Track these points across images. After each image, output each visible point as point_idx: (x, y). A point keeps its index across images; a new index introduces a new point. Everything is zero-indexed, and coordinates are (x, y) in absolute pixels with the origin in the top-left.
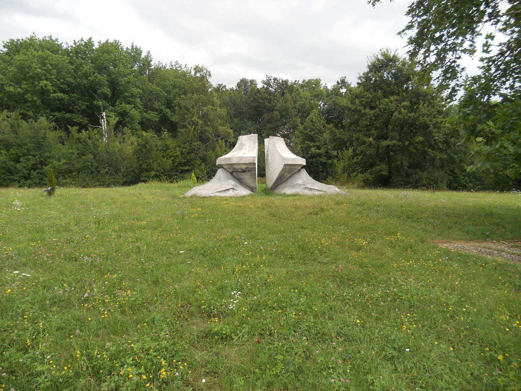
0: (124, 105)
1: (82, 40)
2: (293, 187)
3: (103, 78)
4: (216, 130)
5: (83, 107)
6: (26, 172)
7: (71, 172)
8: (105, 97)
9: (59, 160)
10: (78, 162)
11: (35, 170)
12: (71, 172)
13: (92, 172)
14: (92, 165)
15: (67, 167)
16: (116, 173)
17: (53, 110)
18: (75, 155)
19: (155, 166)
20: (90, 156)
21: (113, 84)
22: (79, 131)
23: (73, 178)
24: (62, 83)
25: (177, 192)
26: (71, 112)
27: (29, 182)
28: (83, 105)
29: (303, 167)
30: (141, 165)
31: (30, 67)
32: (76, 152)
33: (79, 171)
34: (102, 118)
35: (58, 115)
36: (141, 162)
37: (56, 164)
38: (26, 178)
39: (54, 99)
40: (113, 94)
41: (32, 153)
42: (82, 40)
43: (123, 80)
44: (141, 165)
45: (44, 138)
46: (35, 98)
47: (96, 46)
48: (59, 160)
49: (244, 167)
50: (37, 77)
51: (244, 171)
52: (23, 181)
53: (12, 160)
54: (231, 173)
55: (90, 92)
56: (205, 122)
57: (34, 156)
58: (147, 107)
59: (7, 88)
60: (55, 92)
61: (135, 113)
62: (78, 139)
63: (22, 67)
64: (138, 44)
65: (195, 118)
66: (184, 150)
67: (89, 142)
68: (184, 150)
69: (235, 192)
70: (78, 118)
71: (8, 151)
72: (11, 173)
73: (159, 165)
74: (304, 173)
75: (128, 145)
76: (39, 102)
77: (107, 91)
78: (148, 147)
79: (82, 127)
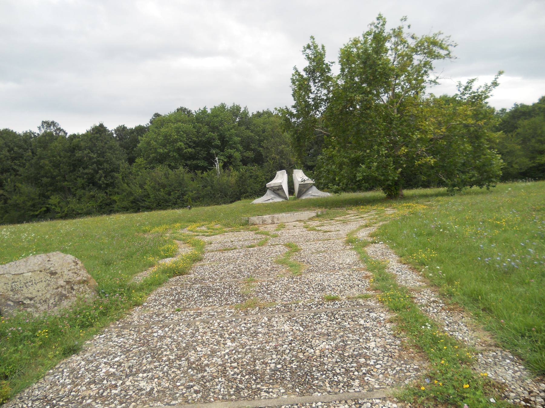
0: (229, 150)
1: (200, 110)
2: (307, 195)
3: (215, 135)
4: (290, 161)
5: (204, 155)
6: (175, 200)
7: (199, 198)
8: (217, 147)
9: (192, 192)
10: (203, 191)
11: (179, 199)
12: (199, 198)
13: (211, 197)
14: (211, 193)
15: (196, 195)
16: (226, 196)
17: (186, 160)
18: (201, 187)
19: (249, 190)
20: (209, 188)
21: (222, 138)
22: (202, 173)
23: (201, 202)
24: (190, 142)
25: (247, 204)
26: (197, 159)
27: (177, 206)
28: (203, 154)
29: (314, 185)
30: (240, 190)
31: (170, 135)
32: (201, 186)
33: (203, 197)
34: (216, 161)
35: (189, 162)
36: (240, 188)
37: (190, 194)
38: (175, 204)
39: (186, 153)
40: (222, 144)
41: (177, 189)
42: (200, 110)
43: (227, 134)
44: (240, 190)
45: (183, 179)
46: (175, 154)
47: (209, 111)
48: (192, 192)
49: (277, 188)
50: (176, 141)
51: (278, 190)
52: (173, 206)
53: (167, 194)
54: (273, 191)
55: (208, 144)
56: (281, 157)
57: (178, 191)
58: (247, 147)
59: (159, 150)
60: (186, 148)
61: (237, 155)
62: (202, 178)
63: (166, 136)
64: (237, 103)
65: (273, 155)
66: (268, 177)
67: (208, 179)
68: (268, 177)
69: (273, 201)
70: (202, 163)
71: (164, 189)
72: (167, 202)
73: (251, 189)
74: (314, 188)
75: (232, 178)
76: (177, 156)
77: (218, 142)
78: (244, 178)
79: (204, 169)
